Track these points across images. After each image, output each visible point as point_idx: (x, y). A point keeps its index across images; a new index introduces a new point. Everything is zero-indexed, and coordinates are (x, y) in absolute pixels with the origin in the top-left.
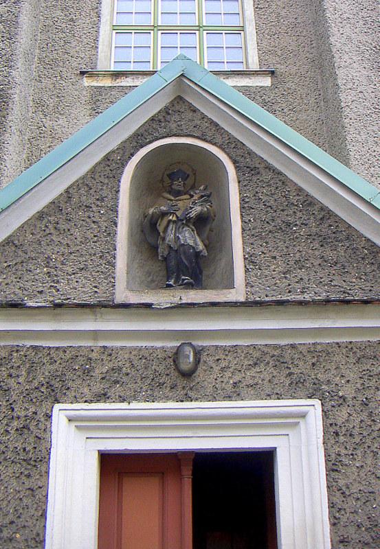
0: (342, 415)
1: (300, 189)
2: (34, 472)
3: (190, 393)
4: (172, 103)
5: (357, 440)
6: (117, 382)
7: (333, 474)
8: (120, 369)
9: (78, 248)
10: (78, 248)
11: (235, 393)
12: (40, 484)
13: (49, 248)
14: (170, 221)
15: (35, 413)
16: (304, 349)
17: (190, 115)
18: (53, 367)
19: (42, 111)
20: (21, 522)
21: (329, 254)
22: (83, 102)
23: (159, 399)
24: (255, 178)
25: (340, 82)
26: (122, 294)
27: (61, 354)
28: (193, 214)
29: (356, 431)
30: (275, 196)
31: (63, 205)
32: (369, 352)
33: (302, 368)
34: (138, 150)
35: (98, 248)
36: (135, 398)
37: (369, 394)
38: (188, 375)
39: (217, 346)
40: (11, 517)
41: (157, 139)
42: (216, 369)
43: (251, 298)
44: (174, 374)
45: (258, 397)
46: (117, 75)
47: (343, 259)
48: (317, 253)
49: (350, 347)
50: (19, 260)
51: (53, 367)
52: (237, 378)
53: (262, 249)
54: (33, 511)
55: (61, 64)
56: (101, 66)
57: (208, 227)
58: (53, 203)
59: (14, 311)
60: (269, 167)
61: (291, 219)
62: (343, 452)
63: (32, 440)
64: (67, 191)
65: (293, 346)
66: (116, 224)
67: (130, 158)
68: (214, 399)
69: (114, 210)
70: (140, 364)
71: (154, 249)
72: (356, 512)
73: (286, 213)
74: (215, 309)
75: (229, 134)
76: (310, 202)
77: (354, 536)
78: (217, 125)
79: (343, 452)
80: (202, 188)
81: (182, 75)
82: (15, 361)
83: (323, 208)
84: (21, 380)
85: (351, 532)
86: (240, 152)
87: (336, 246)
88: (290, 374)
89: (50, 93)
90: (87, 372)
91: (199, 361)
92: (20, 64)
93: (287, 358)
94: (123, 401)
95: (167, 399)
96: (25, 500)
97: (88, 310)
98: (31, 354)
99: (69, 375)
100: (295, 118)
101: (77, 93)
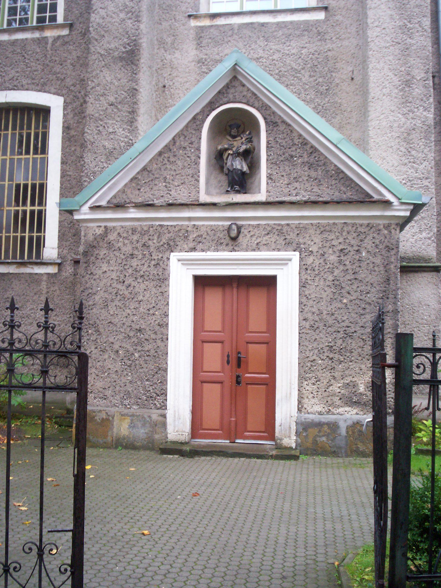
0: (310, 260)
1: (301, 135)
2: (163, 285)
3: (235, 248)
4: (231, 81)
5: (317, 272)
6: (200, 242)
7: (303, 288)
8: (202, 236)
9: (180, 172)
10: (180, 172)
11: (257, 248)
12: (166, 290)
13: (166, 172)
14: (229, 154)
15: (162, 257)
16: (293, 226)
17: (241, 88)
18: (170, 235)
19: (164, 47)
20: (157, 307)
21: (313, 174)
22: (191, 39)
23: (221, 250)
24: (275, 129)
25: (369, 21)
26: (204, 198)
27: (173, 229)
28: (241, 150)
29: (316, 268)
30: (286, 140)
31: (171, 147)
32: (328, 228)
33: (292, 236)
34: (211, 112)
35: (190, 172)
36: (209, 250)
37: (325, 250)
38: (234, 239)
39: (249, 225)
40: (153, 305)
41: (222, 105)
42: (249, 236)
43: (271, 199)
44: (228, 238)
45: (269, 250)
46: (214, 16)
47: (319, 177)
48: (306, 173)
49: (318, 226)
50: (150, 179)
51: (170, 235)
52: (258, 240)
53: (277, 171)
54: (163, 302)
55: (174, 9)
56: (203, 10)
57: (250, 157)
58: (166, 146)
59: (150, 208)
60: (284, 122)
61: (294, 153)
62: (309, 278)
63: (161, 270)
64: (173, 139)
65: (288, 225)
66: (199, 158)
67: (207, 118)
68: (247, 251)
69: (198, 149)
70: (211, 233)
71: (222, 168)
72: (312, 307)
73: (291, 150)
74: (248, 206)
75: (262, 101)
76: (305, 143)
77: (311, 318)
78: (255, 95)
79: (309, 278)
80: (247, 133)
81: (236, 64)
82: (151, 232)
83: (312, 147)
84: (155, 241)
85: (309, 316)
86: (268, 112)
87: (317, 169)
88: (285, 239)
89: (168, 33)
90: (186, 237)
91: (240, 232)
92: (145, 18)
93: (284, 231)
94: (203, 251)
95: (224, 250)
96: (159, 297)
97: (185, 207)
98: (159, 228)
99: (178, 239)
100: (339, 45)
101: (186, 32)
